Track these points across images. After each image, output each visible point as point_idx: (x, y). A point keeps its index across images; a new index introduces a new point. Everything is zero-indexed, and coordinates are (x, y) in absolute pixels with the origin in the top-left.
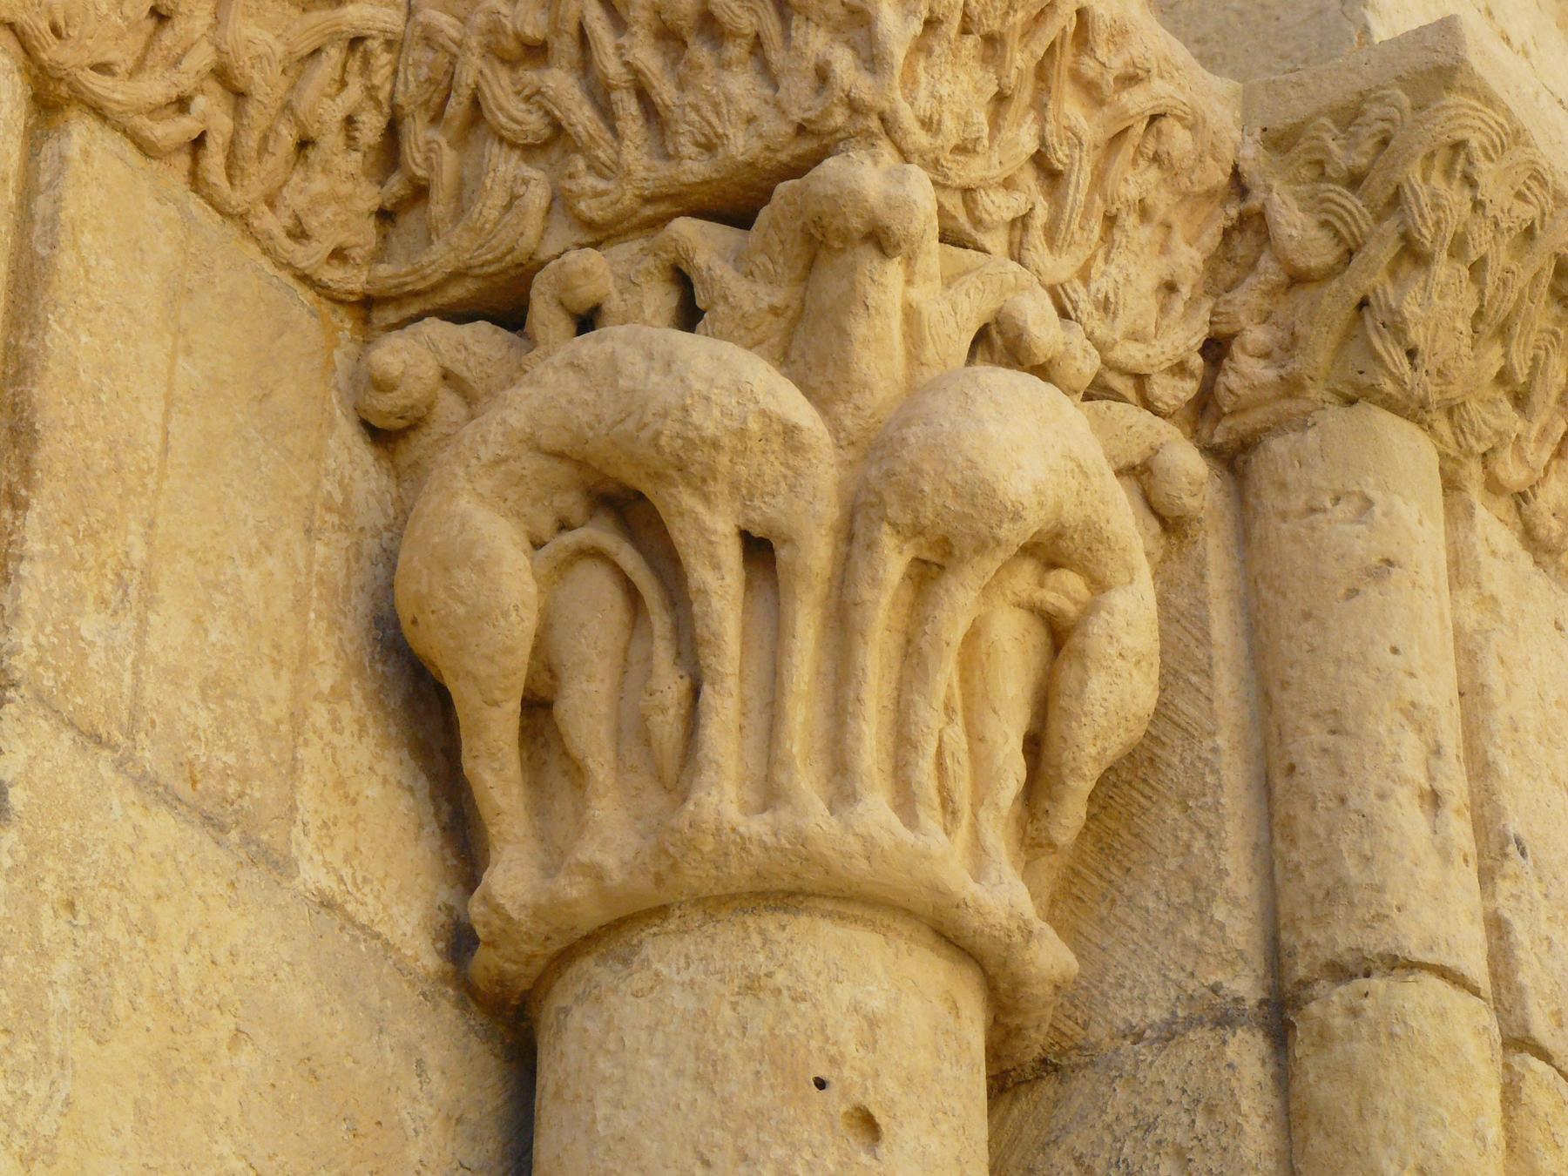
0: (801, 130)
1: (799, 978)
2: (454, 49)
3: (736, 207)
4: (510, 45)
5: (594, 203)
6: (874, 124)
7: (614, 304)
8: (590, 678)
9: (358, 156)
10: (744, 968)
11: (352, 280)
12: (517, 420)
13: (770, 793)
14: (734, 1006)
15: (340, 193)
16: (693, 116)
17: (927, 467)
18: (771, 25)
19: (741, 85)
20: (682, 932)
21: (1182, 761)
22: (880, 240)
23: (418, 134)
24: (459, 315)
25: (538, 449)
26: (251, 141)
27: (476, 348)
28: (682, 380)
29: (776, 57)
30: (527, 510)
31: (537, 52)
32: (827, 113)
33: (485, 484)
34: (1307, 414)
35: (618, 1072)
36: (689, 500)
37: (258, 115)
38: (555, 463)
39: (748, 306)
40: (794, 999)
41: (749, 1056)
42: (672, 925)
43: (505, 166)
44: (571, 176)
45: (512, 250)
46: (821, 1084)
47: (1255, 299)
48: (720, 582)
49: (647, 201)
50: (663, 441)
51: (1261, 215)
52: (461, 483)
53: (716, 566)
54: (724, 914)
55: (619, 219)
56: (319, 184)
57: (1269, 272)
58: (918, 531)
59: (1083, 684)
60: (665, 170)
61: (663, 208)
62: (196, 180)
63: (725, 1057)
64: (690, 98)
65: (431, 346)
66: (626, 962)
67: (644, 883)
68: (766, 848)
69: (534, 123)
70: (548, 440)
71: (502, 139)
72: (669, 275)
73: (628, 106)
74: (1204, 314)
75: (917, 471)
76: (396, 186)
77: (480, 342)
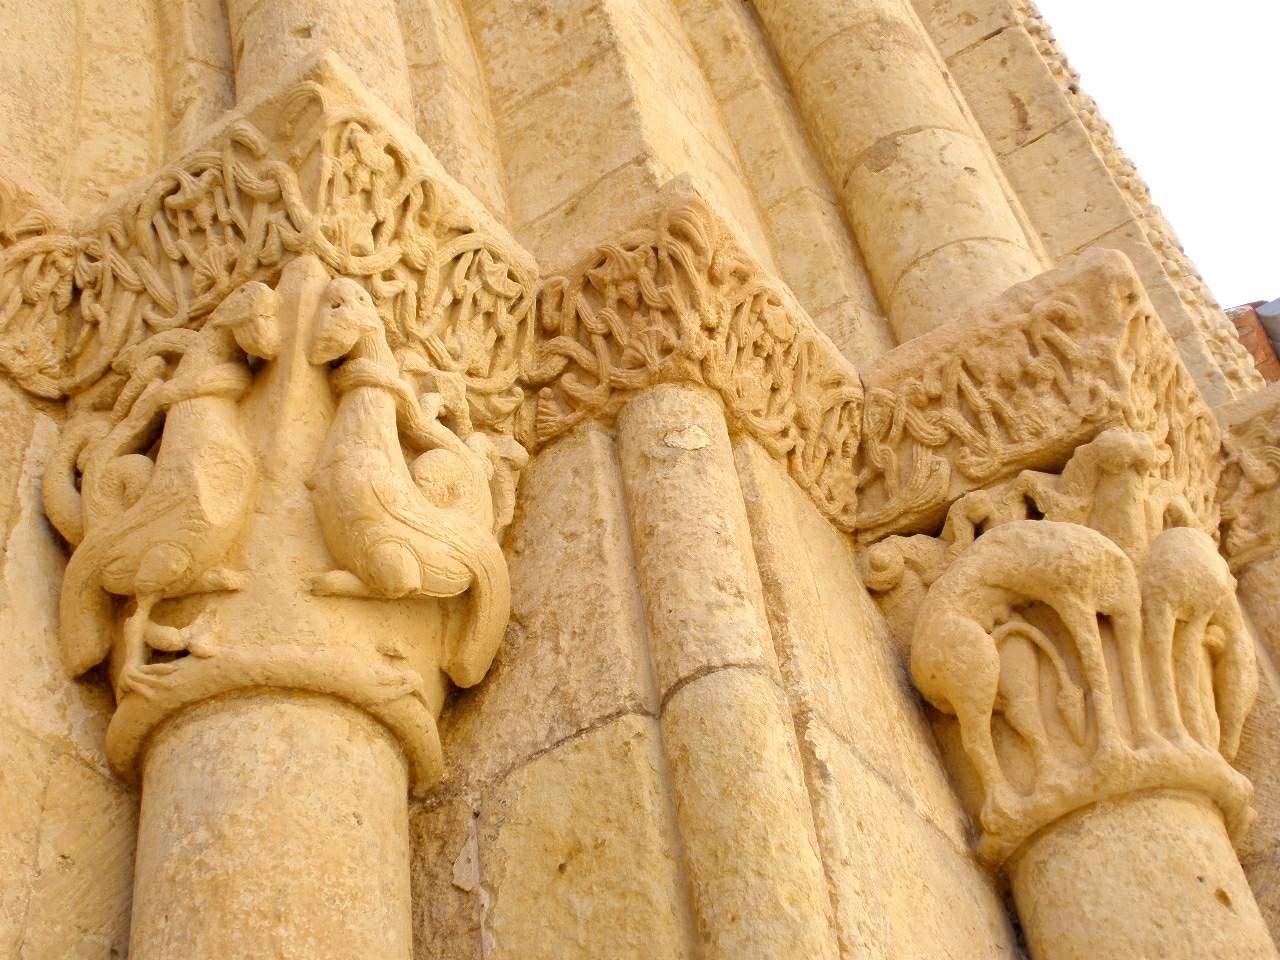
0: (1085, 421)
1: (1172, 829)
2: (892, 404)
3: (1054, 465)
4: (923, 398)
5: (978, 468)
6: (1120, 413)
7: (996, 515)
8: (1027, 695)
9: (849, 460)
10: (1144, 828)
11: (850, 521)
12: (972, 571)
13: (1138, 740)
14: (1146, 847)
15: (842, 475)
16: (1027, 420)
17: (1184, 571)
18: (1061, 374)
19: (1050, 402)
20: (1104, 814)
21: (1262, 714)
22: (1138, 466)
23: (876, 448)
24: (908, 533)
25: (985, 584)
26: (810, 451)
27: (921, 546)
28: (1064, 540)
29: (1067, 388)
30: (981, 616)
31: (935, 401)
32: (1099, 410)
33: (960, 605)
34: (1273, 552)
35: (1091, 888)
36: (1073, 599)
37: (812, 436)
38: (993, 590)
39: (1070, 507)
40: (1174, 840)
41: (1162, 870)
42: (1098, 811)
43: (926, 457)
44: (963, 457)
45: (935, 497)
46: (1201, 879)
47: (1240, 501)
48: (1091, 637)
49: (1004, 464)
50: (1061, 570)
51: (1237, 464)
52: (947, 605)
53: (1090, 631)
54: (1125, 802)
55: (993, 474)
56: (837, 474)
57: (1245, 487)
58: (1181, 604)
59: (1238, 677)
60: (1014, 448)
61: (1013, 467)
62: (791, 470)
63: (1151, 872)
64: (1023, 412)
65: (897, 546)
66: (1077, 833)
67: (1088, 791)
68: (1148, 765)
69: (940, 434)
70: (991, 579)
71: (922, 444)
72: (1021, 499)
73: (989, 421)
74: (1218, 512)
75: (1180, 574)
76: (866, 473)
77: (922, 544)
